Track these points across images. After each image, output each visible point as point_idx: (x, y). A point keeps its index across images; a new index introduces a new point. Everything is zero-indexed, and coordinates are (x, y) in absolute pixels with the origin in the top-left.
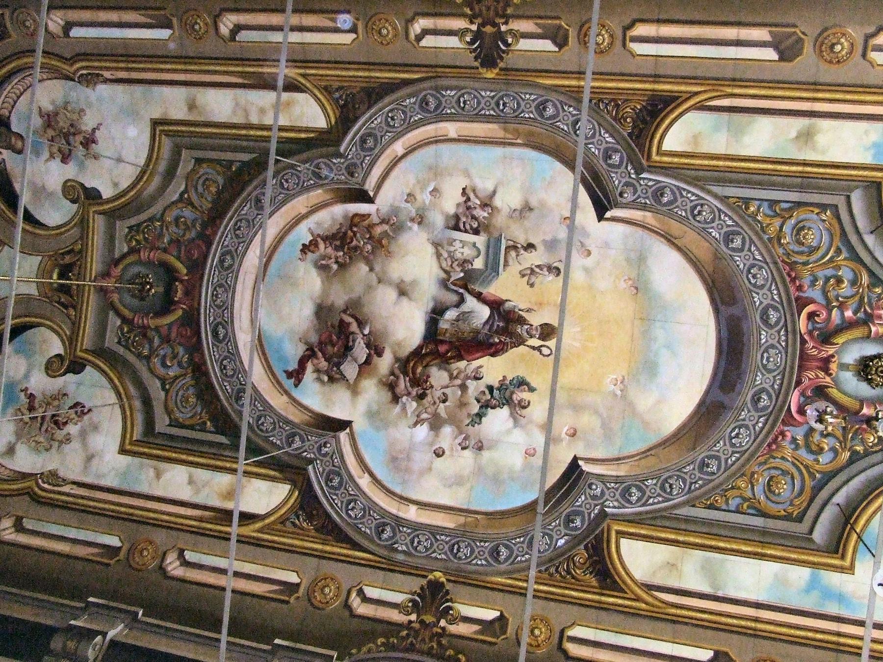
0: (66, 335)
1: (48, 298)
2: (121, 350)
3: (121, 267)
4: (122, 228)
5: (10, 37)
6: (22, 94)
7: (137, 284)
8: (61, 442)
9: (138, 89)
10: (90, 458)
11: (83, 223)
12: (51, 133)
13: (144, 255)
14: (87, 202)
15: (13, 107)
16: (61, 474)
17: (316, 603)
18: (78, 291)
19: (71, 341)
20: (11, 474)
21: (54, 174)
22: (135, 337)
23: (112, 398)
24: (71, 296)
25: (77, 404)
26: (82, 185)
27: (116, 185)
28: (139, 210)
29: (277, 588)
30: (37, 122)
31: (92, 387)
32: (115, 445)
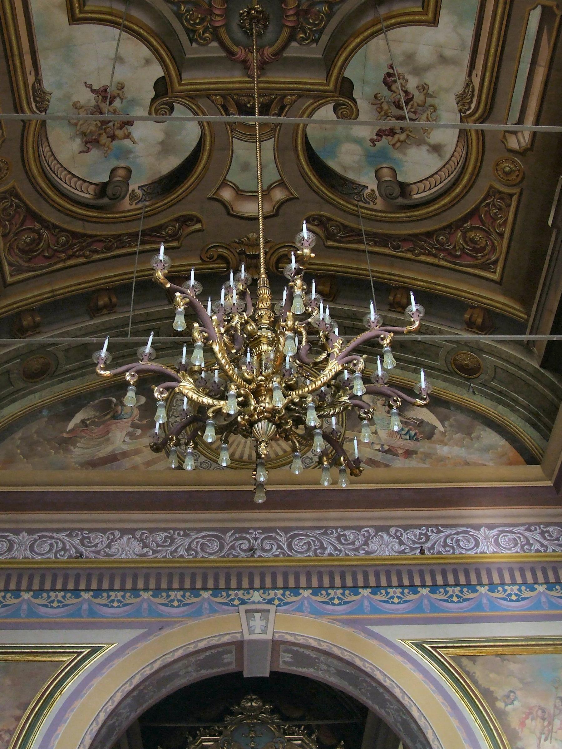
0: (313, 104)
1: (276, 127)
2: (325, 38)
3: (235, 49)
4: (193, 51)
5: (14, 187)
6: (70, 173)
7: (251, 25)
8: (427, 95)
9: (41, 42)
10: (443, 60)
11: (193, 97)
12: (104, 139)
13: (219, 22)
14: (170, 94)
15: (85, 181)
16: (459, 89)
17: (519, 179)
18: (266, 95)
19: (320, 97)
20: (460, 145)
21: (146, 134)
22: (309, 24)
23: (378, 42)
24: (272, 101)
25: (386, 83)
26: (153, 100)
27: (148, 62)
28: (172, 33)
29: (545, 30)
30: (95, 153)
31: (365, 68)
32: (428, 32)
